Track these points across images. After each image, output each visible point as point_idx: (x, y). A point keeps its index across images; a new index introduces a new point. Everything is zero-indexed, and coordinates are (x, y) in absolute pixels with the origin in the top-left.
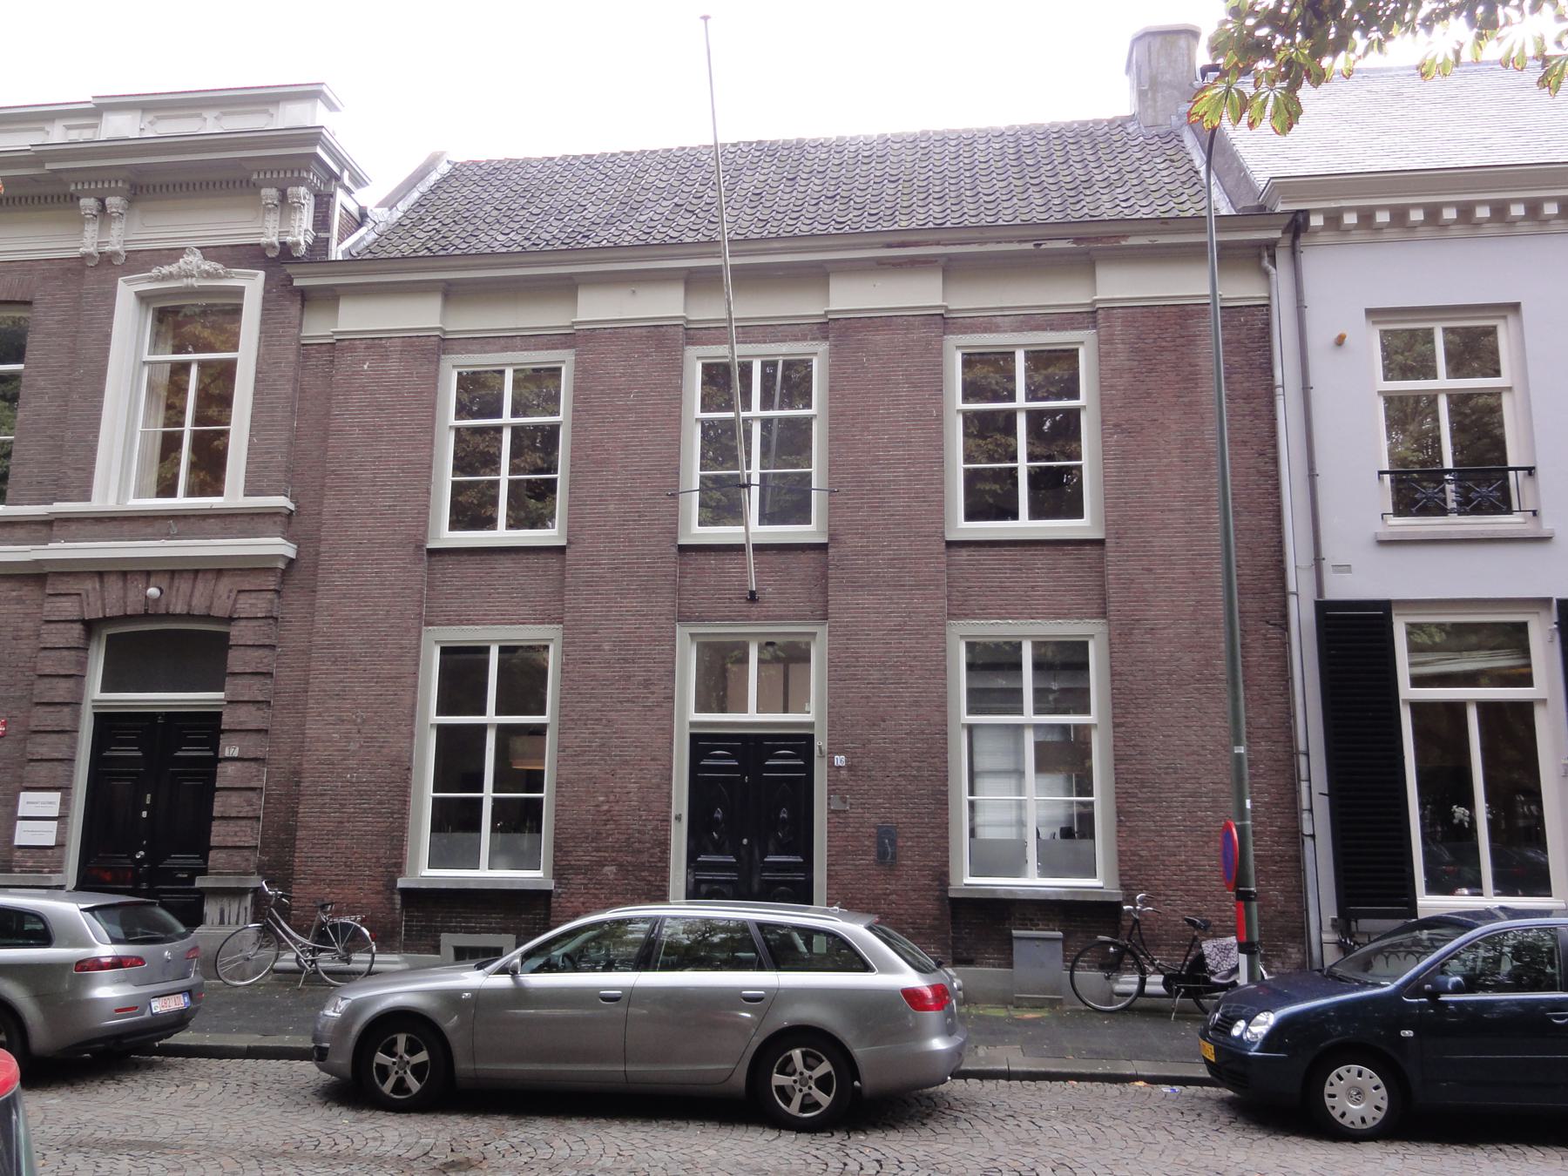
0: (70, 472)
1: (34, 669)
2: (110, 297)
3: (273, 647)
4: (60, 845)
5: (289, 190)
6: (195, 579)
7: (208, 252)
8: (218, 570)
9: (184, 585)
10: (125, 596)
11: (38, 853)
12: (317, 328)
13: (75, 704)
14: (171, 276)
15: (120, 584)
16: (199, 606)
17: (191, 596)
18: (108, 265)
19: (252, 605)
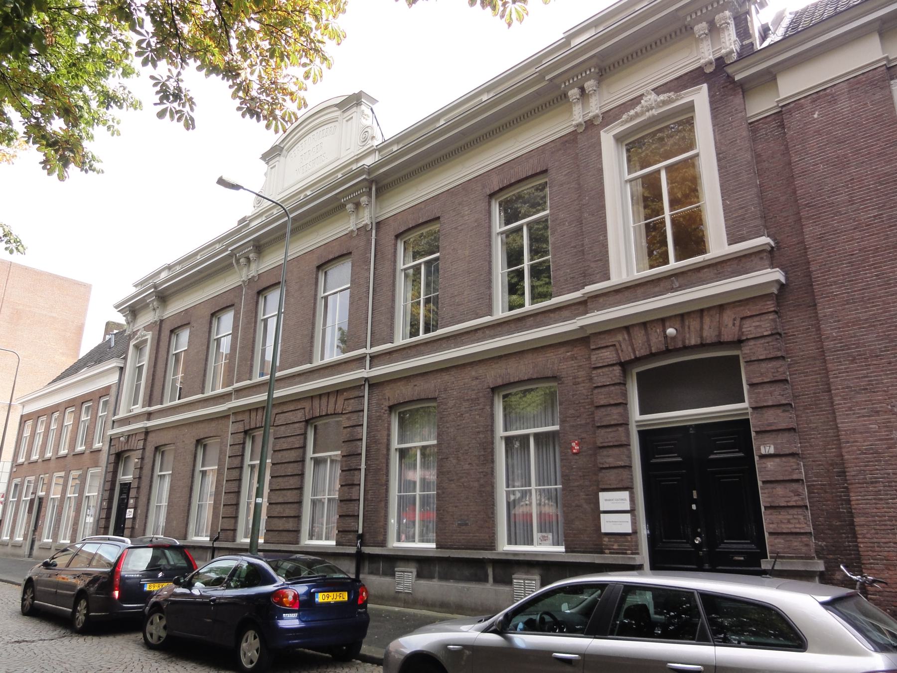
0: (593, 265)
1: (592, 403)
2: (597, 146)
3: (783, 358)
4: (635, 532)
5: (585, 86)
6: (702, 317)
7: (658, 91)
8: (718, 307)
9: (694, 324)
10: (648, 340)
11: (621, 539)
12: (761, 106)
13: (625, 424)
14: (637, 115)
15: (698, 320)
16: (709, 334)
17: (702, 329)
18: (591, 126)
19: (757, 327)
